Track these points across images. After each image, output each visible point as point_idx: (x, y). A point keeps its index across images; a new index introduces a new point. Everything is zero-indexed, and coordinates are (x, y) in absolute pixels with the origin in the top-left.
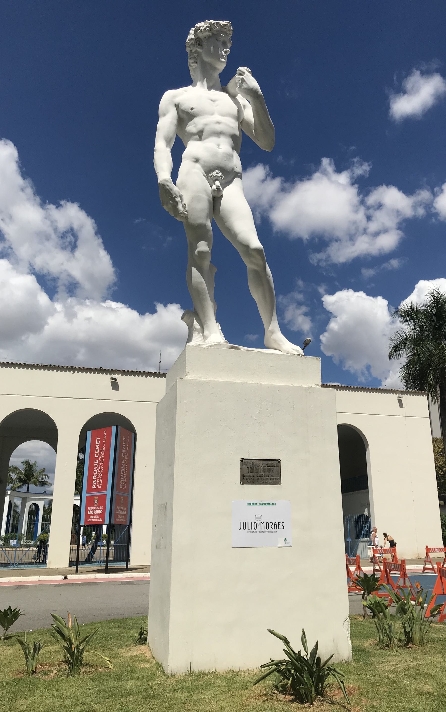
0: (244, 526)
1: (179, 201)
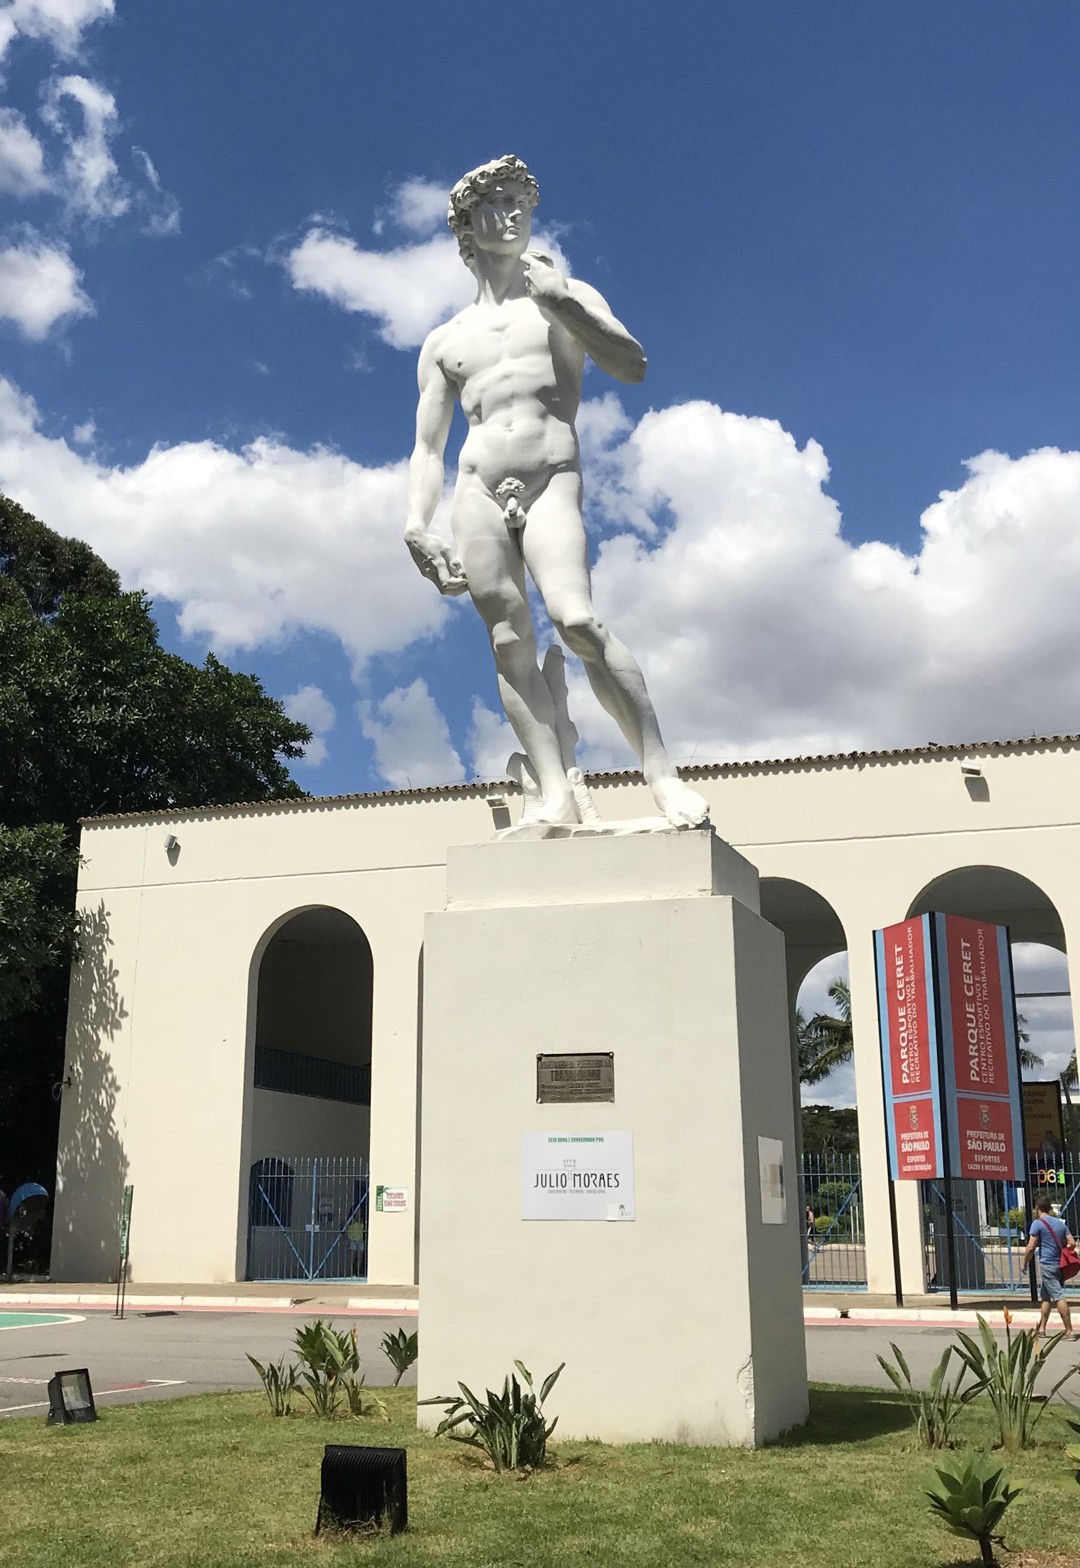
0: (542, 1181)
1: (439, 565)
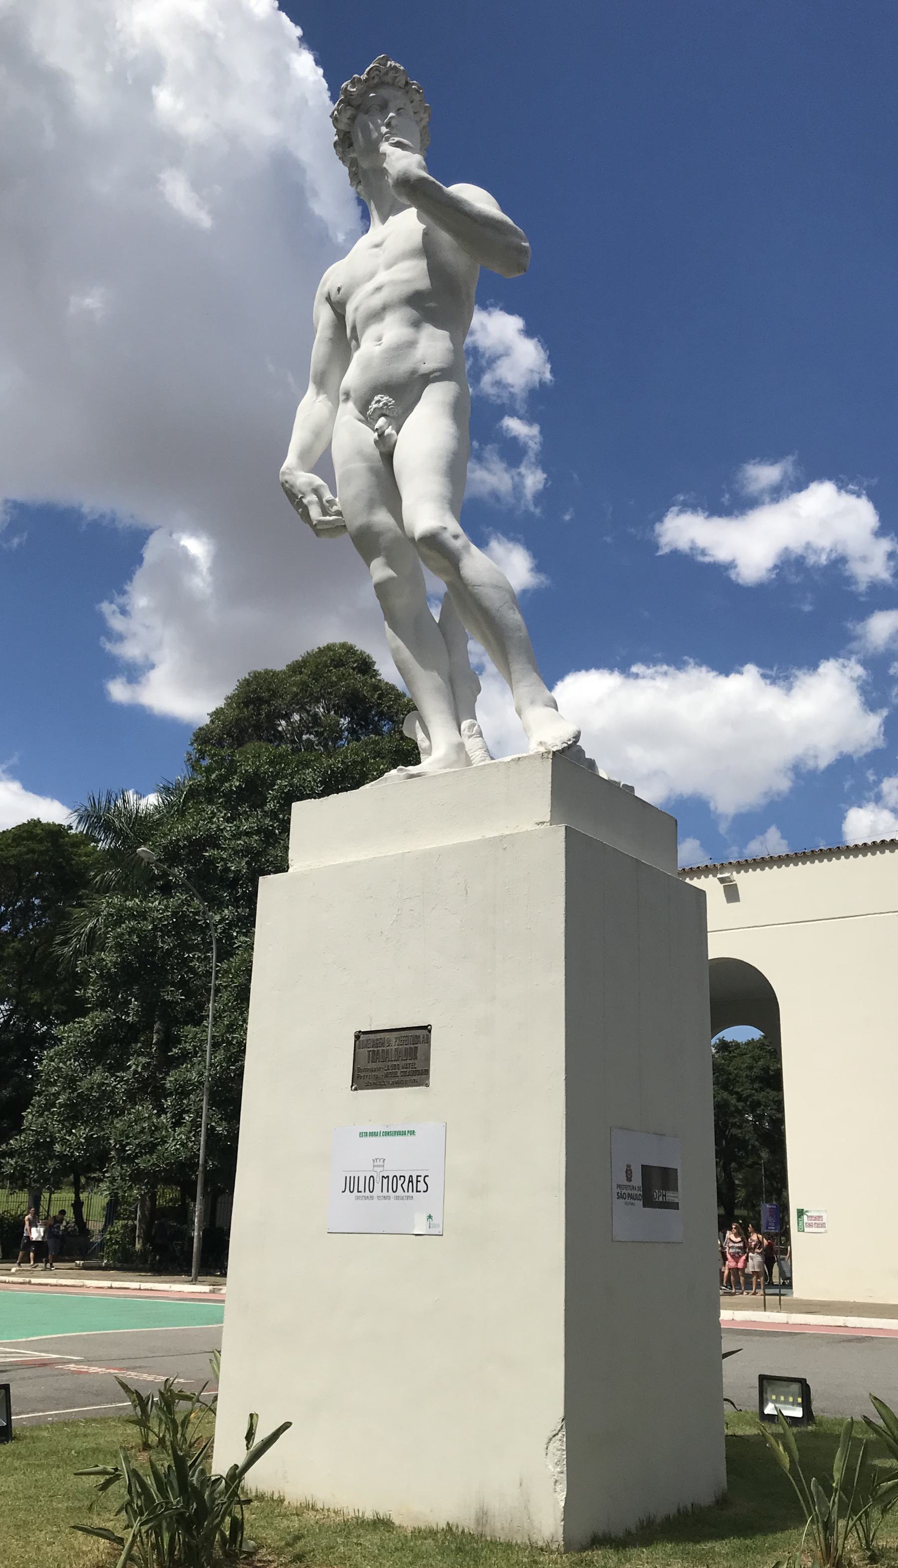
1: (310, 502)
